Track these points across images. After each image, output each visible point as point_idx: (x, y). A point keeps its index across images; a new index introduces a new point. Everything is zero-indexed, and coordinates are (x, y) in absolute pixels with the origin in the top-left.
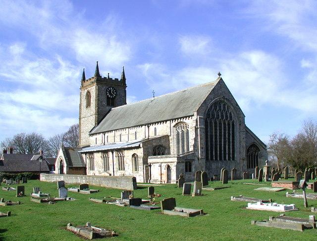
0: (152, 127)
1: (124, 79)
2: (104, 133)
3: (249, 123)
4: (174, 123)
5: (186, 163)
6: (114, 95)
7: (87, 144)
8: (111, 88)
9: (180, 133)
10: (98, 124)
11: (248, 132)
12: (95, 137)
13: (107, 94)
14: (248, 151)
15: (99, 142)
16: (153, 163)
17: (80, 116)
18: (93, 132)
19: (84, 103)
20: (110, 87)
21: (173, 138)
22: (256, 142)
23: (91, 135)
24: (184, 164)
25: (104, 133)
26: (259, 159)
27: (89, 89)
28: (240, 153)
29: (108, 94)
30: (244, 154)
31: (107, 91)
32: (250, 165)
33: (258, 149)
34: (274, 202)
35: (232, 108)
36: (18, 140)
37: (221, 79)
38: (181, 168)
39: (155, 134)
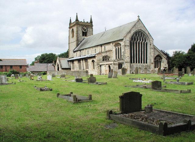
0: (103, 47)
1: (91, 22)
2: (102, 53)
4: (114, 44)
5: (119, 64)
7: (73, 57)
9: (117, 49)
10: (78, 46)
12: (76, 53)
14: (155, 59)
15: (78, 55)
16: (102, 65)
17: (69, 42)
18: (75, 50)
19: (71, 35)
23: (74, 52)
25: (80, 50)
30: (153, 61)
31: (82, 28)
32: (156, 65)
34: (26, 28)
35: (146, 35)
36: (52, 54)
37: (140, 19)
39: (105, 50)
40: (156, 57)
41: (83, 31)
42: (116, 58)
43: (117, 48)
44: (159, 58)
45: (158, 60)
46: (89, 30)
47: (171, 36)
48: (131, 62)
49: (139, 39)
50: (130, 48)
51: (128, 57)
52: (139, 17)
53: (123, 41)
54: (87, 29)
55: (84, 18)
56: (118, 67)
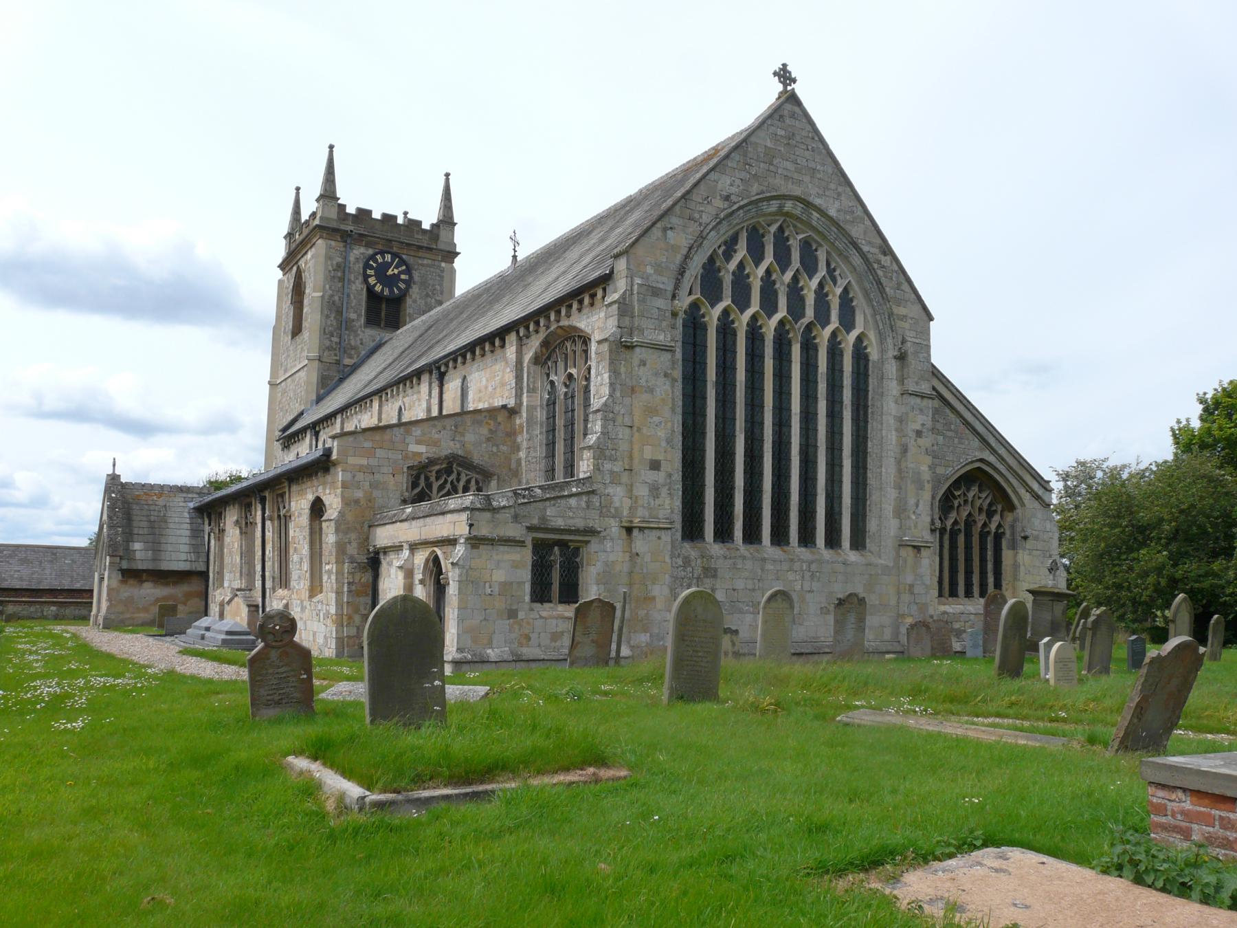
1: (447, 221)
3: (953, 352)
5: (541, 549)
6: (402, 286)
8: (388, 257)
11: (947, 402)
13: (366, 277)
14: (946, 503)
20: (382, 253)
21: (530, 420)
22: (992, 459)
24: (525, 556)
26: (1007, 555)
27: (1144, 670)
28: (902, 505)
29: (372, 281)
31: (367, 266)
33: (1003, 500)
38: (499, 576)
40: (957, 484)
41: (370, 290)
42: (550, 472)
43: (558, 379)
44: (985, 499)
45: (970, 522)
46: (422, 267)
47: (1064, 355)
48: (692, 528)
49: (782, 302)
50: (678, 374)
51: (655, 465)
52: (784, 75)
53: (613, 297)
54: (408, 271)
55: (388, 188)
56: (525, 575)
